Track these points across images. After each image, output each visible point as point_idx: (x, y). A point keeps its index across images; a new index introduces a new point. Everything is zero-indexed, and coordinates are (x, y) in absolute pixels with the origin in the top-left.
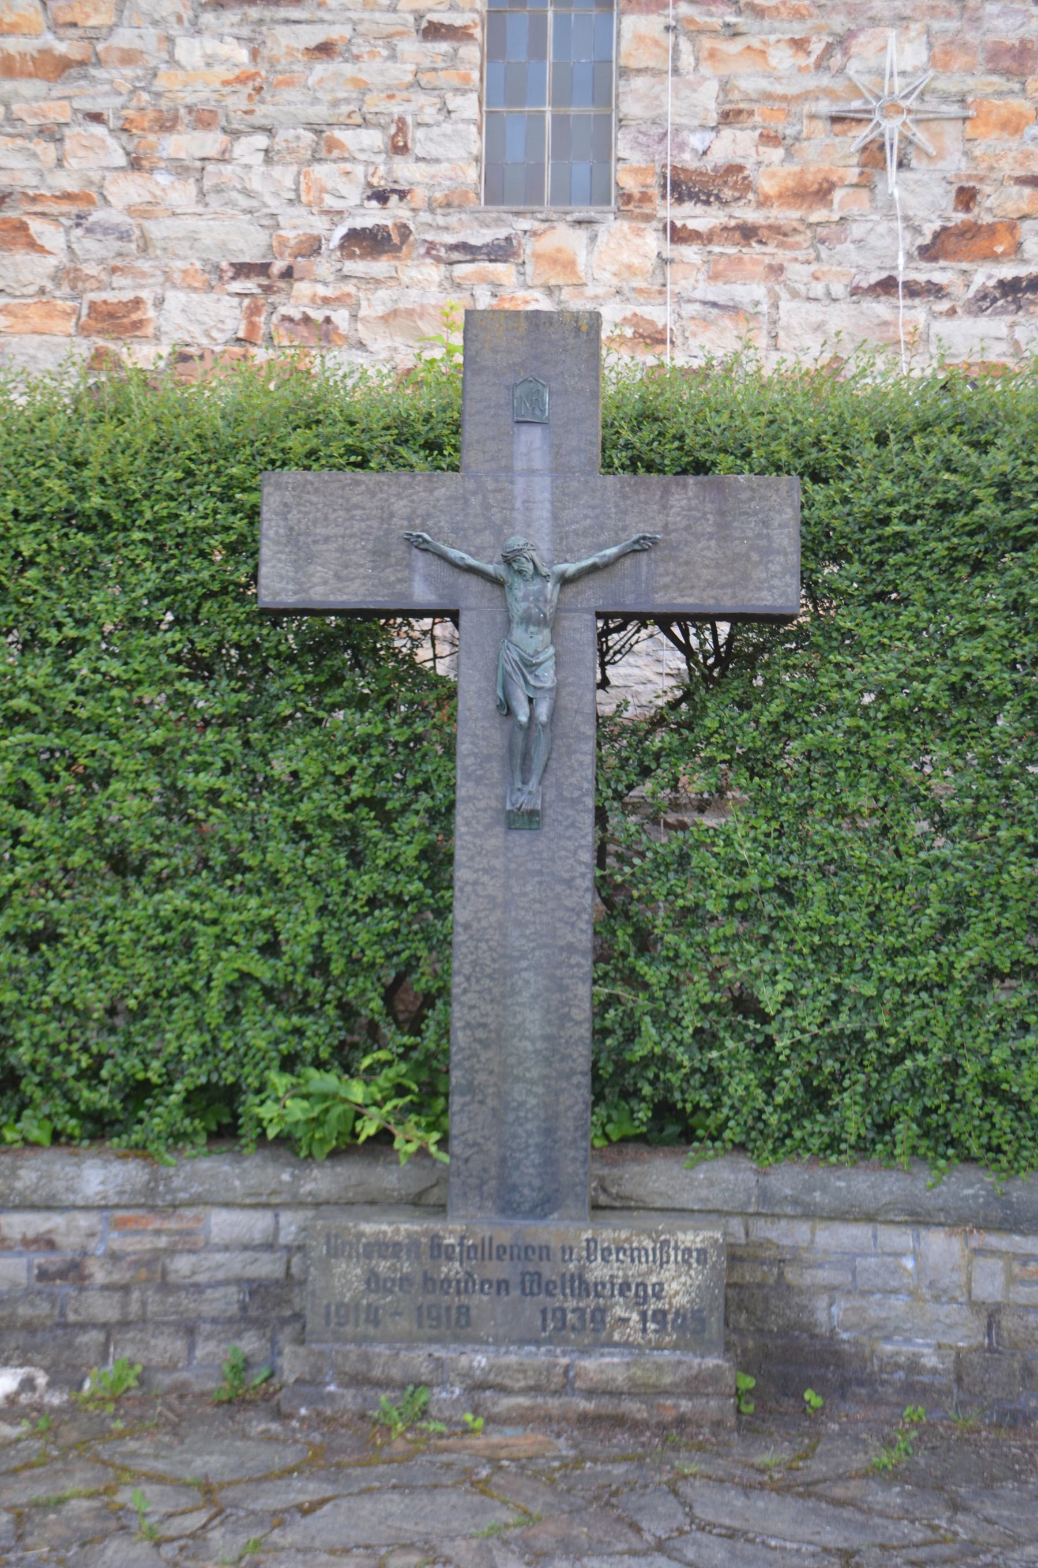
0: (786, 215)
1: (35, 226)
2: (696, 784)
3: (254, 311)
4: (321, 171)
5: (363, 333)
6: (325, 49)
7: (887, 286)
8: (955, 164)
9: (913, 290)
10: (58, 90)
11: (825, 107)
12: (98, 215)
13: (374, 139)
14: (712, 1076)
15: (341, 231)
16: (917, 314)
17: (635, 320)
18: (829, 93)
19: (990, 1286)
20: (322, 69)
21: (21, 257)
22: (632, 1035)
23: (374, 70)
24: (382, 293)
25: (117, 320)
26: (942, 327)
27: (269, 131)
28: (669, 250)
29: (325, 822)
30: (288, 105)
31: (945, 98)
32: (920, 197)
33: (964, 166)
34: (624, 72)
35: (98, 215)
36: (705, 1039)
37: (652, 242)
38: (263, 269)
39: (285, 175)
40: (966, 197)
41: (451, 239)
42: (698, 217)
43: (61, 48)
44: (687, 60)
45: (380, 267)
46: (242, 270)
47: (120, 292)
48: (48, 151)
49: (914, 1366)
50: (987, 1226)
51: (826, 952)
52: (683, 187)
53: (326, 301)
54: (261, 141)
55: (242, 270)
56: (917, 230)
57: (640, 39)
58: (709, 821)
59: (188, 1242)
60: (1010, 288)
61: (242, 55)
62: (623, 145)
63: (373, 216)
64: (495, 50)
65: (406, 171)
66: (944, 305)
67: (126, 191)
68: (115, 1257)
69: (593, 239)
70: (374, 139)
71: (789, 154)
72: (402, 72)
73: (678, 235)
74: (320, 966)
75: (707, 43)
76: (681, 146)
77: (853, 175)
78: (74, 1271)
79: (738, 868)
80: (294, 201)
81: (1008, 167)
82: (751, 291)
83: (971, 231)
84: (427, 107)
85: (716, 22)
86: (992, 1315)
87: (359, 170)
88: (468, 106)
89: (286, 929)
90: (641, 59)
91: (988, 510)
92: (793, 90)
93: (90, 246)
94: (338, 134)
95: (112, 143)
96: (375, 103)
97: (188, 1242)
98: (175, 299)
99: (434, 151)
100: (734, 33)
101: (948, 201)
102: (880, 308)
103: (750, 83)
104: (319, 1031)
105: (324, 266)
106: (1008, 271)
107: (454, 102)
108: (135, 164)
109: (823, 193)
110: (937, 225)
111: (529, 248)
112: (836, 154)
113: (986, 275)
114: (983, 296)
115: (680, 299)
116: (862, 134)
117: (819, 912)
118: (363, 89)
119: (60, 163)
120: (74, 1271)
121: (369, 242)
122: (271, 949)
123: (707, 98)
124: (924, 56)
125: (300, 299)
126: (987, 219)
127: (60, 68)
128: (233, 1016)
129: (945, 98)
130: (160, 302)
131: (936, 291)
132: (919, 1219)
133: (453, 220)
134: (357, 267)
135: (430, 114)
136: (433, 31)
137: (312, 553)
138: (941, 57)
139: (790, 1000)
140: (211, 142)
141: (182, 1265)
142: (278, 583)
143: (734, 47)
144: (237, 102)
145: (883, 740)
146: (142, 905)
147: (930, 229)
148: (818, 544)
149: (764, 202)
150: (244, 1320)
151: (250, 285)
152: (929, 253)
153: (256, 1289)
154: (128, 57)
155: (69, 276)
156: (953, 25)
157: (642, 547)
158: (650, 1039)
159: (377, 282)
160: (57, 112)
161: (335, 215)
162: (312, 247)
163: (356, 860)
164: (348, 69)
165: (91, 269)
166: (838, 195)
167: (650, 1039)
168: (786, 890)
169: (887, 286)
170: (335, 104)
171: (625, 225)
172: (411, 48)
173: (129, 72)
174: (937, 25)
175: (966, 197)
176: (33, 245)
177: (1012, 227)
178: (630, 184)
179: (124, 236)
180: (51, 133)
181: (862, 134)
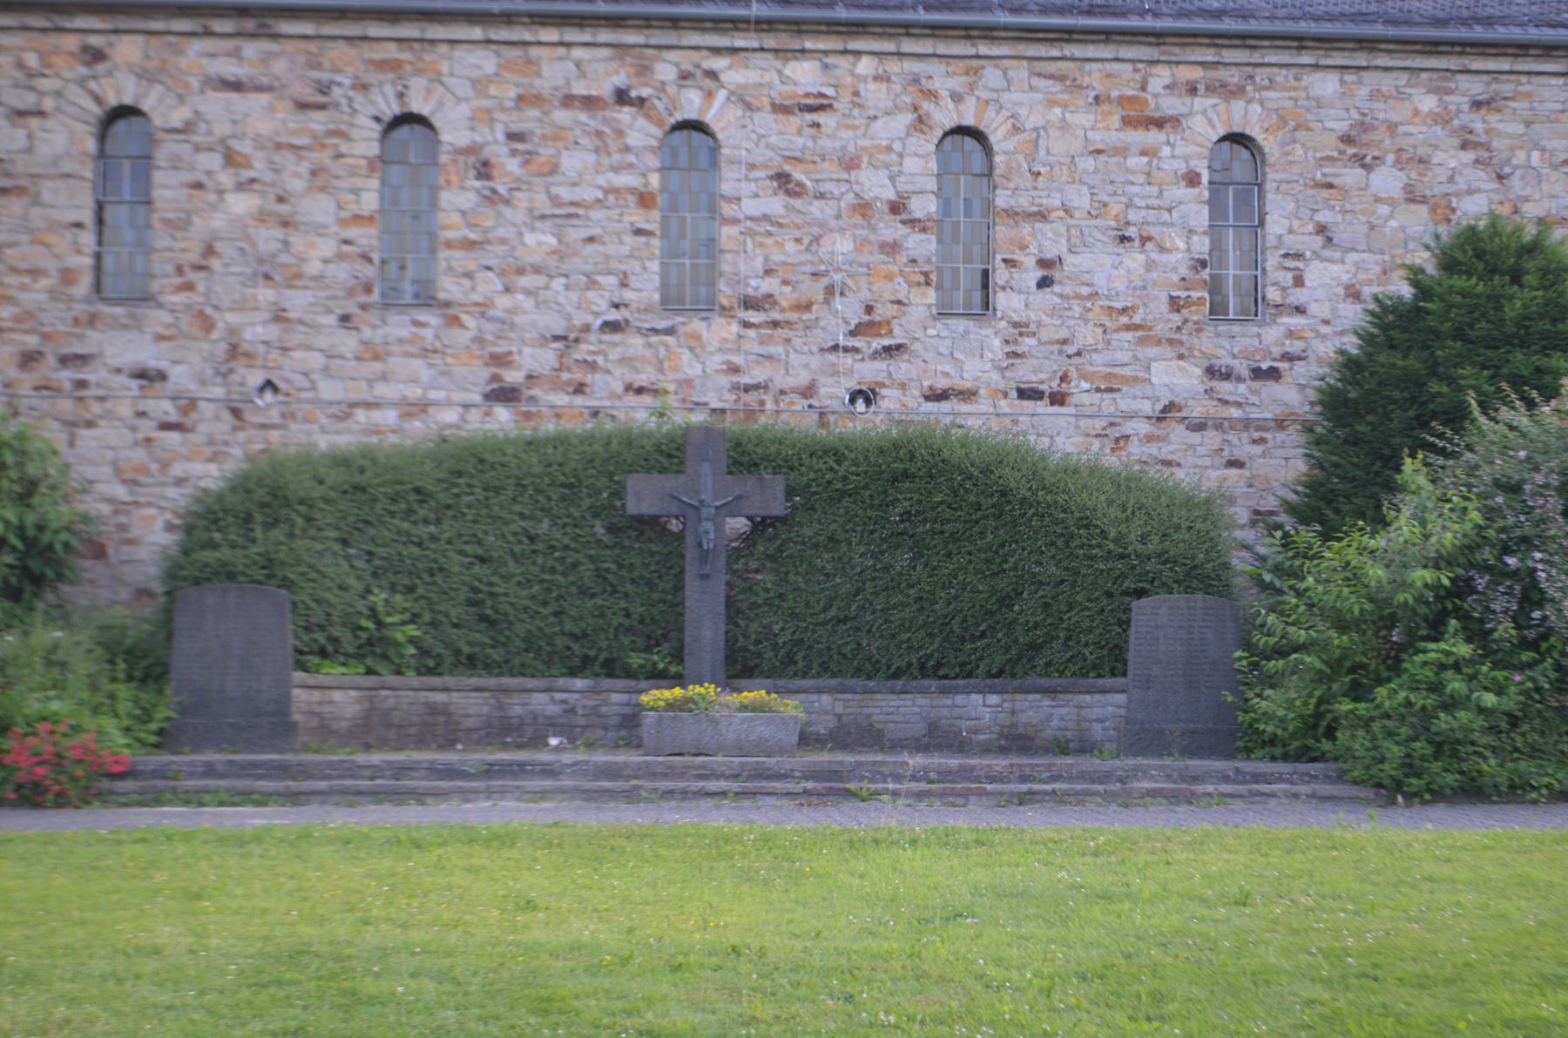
0: (793, 316)
1: (464, 317)
2: (754, 564)
3: (561, 356)
4: (591, 294)
5: (610, 366)
6: (591, 239)
7: (835, 348)
8: (865, 295)
9: (846, 350)
10: (472, 255)
11: (809, 269)
12: (491, 313)
13: (613, 280)
14: (759, 654)
15: (599, 322)
16: (847, 360)
17: (727, 363)
18: (812, 263)
19: (839, 709)
20: (590, 248)
21: (457, 331)
22: (736, 641)
23: (612, 249)
24: (619, 350)
25: (501, 360)
26: (858, 366)
27: (566, 276)
28: (743, 332)
29: (642, 577)
30: (575, 263)
31: (861, 265)
32: (849, 309)
33: (868, 295)
34: (721, 251)
35: (491, 313)
36: (758, 642)
37: (735, 328)
38: (564, 338)
39: (574, 296)
40: (869, 309)
41: (647, 326)
42: (754, 317)
43: (472, 236)
44: (750, 247)
45: (617, 337)
46: (557, 338)
47: (501, 348)
48: (466, 283)
49: (818, 734)
50: (839, 692)
51: (794, 616)
52: (749, 303)
53: (594, 353)
54: (563, 280)
55: (557, 338)
56: (848, 323)
57: (729, 237)
58: (759, 577)
59: (606, 703)
60: (887, 349)
61: (553, 241)
62: (722, 285)
63: (614, 315)
64: (665, 235)
65: (628, 295)
66: (859, 357)
67: (504, 302)
68: (584, 707)
69: (709, 326)
70: (613, 280)
71: (794, 289)
72: (625, 250)
73: (746, 325)
74: (641, 622)
75: (759, 239)
76: (747, 285)
77: (821, 298)
78: (573, 711)
79: (767, 590)
80: (579, 308)
81: (888, 296)
82: (777, 350)
83: (871, 324)
84: (635, 266)
85: (762, 230)
86: (839, 717)
87: (606, 294)
88: (655, 266)
89: (632, 610)
90: (730, 246)
91: (839, 486)
92: (795, 261)
93: (489, 327)
94: (599, 278)
95: (496, 280)
96: (614, 265)
97: (606, 703)
98: (527, 351)
99: (640, 286)
100: (770, 234)
101: (861, 311)
102: (832, 357)
103: (777, 257)
104: (641, 643)
105: (592, 337)
106: (886, 342)
107: (649, 264)
108: (508, 290)
109: (807, 307)
110: (856, 321)
111: (682, 330)
112: (815, 290)
113: (878, 343)
114: (876, 352)
115: (747, 353)
116: (825, 281)
117: (791, 603)
118: (607, 257)
119: (473, 289)
120: (573, 711)
121: (612, 327)
122: (628, 616)
123: (758, 264)
124: (852, 246)
125: (582, 351)
126: (878, 319)
127: (469, 245)
128: (616, 636)
129: (861, 265)
130: (520, 352)
131: (856, 350)
132: (819, 691)
133: (648, 317)
134: (607, 337)
135: (638, 269)
136: (639, 232)
137: (644, 495)
138: (860, 245)
139: (782, 629)
140: (540, 280)
141: (604, 709)
142: (633, 507)
143: (769, 241)
144: (552, 262)
145: (809, 552)
146: (589, 604)
147: (854, 322)
148: (790, 492)
149: (783, 310)
150: (621, 726)
151: (559, 345)
152: (853, 333)
153: (625, 717)
154: (503, 241)
155: (479, 340)
156: (865, 232)
157: (739, 498)
158: (741, 642)
159: (614, 344)
160: (471, 266)
161: (596, 314)
162: (586, 328)
163: (651, 589)
164: (601, 248)
165: (489, 337)
166: (814, 308)
167: (741, 642)
168: (780, 596)
169: (835, 348)
170: (596, 264)
171: (722, 321)
172: (629, 239)
173: (503, 248)
174: (858, 232)
175: (869, 309)
176: (462, 326)
177: (888, 323)
178: (725, 302)
179: (503, 322)
180: (469, 275)
181: (825, 281)
